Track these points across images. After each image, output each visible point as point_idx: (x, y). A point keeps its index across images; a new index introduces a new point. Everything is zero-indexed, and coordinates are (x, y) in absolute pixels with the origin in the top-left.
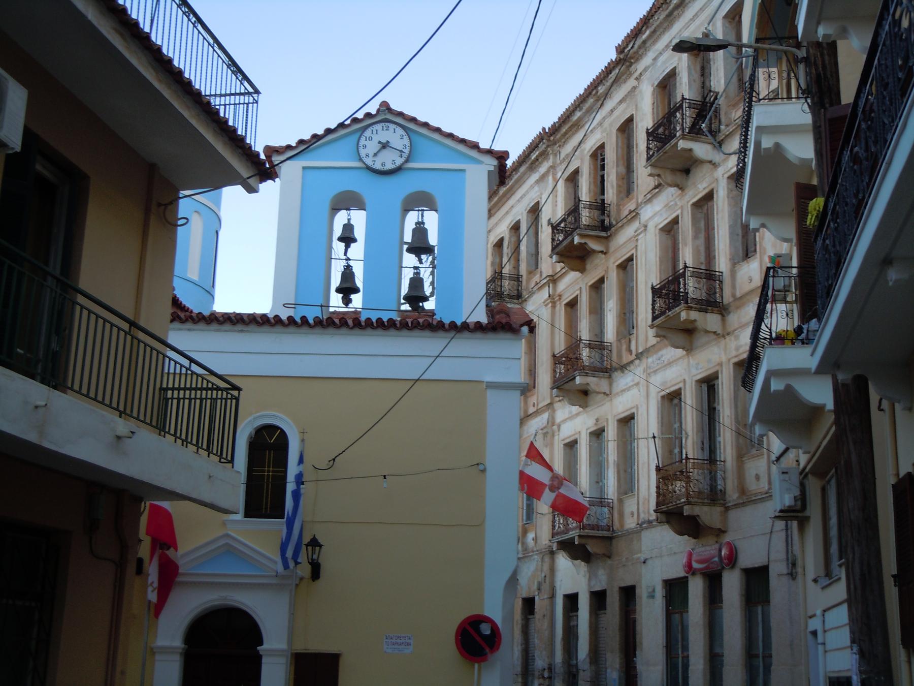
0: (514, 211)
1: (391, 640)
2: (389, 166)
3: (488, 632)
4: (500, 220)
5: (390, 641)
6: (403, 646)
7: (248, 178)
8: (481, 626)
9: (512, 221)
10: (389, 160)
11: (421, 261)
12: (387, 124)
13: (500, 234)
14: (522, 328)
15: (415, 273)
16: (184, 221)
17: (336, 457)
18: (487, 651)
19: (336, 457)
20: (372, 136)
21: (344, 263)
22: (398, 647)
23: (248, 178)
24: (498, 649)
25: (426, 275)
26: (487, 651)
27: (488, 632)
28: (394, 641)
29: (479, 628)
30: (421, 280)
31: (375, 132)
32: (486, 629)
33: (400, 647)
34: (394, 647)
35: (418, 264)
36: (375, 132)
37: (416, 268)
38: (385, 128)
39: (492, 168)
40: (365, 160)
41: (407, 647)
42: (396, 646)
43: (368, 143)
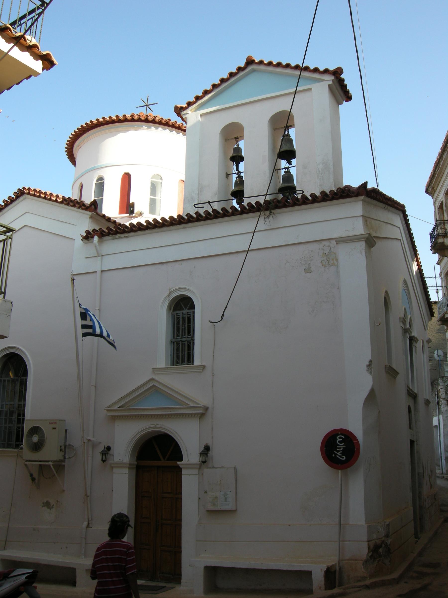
9: (445, 190)
11: (290, 163)
15: (285, 172)
17: (224, 312)
19: (224, 312)
25: (293, 171)
30: (292, 176)
35: (288, 165)
37: (288, 168)
39: (331, 82)
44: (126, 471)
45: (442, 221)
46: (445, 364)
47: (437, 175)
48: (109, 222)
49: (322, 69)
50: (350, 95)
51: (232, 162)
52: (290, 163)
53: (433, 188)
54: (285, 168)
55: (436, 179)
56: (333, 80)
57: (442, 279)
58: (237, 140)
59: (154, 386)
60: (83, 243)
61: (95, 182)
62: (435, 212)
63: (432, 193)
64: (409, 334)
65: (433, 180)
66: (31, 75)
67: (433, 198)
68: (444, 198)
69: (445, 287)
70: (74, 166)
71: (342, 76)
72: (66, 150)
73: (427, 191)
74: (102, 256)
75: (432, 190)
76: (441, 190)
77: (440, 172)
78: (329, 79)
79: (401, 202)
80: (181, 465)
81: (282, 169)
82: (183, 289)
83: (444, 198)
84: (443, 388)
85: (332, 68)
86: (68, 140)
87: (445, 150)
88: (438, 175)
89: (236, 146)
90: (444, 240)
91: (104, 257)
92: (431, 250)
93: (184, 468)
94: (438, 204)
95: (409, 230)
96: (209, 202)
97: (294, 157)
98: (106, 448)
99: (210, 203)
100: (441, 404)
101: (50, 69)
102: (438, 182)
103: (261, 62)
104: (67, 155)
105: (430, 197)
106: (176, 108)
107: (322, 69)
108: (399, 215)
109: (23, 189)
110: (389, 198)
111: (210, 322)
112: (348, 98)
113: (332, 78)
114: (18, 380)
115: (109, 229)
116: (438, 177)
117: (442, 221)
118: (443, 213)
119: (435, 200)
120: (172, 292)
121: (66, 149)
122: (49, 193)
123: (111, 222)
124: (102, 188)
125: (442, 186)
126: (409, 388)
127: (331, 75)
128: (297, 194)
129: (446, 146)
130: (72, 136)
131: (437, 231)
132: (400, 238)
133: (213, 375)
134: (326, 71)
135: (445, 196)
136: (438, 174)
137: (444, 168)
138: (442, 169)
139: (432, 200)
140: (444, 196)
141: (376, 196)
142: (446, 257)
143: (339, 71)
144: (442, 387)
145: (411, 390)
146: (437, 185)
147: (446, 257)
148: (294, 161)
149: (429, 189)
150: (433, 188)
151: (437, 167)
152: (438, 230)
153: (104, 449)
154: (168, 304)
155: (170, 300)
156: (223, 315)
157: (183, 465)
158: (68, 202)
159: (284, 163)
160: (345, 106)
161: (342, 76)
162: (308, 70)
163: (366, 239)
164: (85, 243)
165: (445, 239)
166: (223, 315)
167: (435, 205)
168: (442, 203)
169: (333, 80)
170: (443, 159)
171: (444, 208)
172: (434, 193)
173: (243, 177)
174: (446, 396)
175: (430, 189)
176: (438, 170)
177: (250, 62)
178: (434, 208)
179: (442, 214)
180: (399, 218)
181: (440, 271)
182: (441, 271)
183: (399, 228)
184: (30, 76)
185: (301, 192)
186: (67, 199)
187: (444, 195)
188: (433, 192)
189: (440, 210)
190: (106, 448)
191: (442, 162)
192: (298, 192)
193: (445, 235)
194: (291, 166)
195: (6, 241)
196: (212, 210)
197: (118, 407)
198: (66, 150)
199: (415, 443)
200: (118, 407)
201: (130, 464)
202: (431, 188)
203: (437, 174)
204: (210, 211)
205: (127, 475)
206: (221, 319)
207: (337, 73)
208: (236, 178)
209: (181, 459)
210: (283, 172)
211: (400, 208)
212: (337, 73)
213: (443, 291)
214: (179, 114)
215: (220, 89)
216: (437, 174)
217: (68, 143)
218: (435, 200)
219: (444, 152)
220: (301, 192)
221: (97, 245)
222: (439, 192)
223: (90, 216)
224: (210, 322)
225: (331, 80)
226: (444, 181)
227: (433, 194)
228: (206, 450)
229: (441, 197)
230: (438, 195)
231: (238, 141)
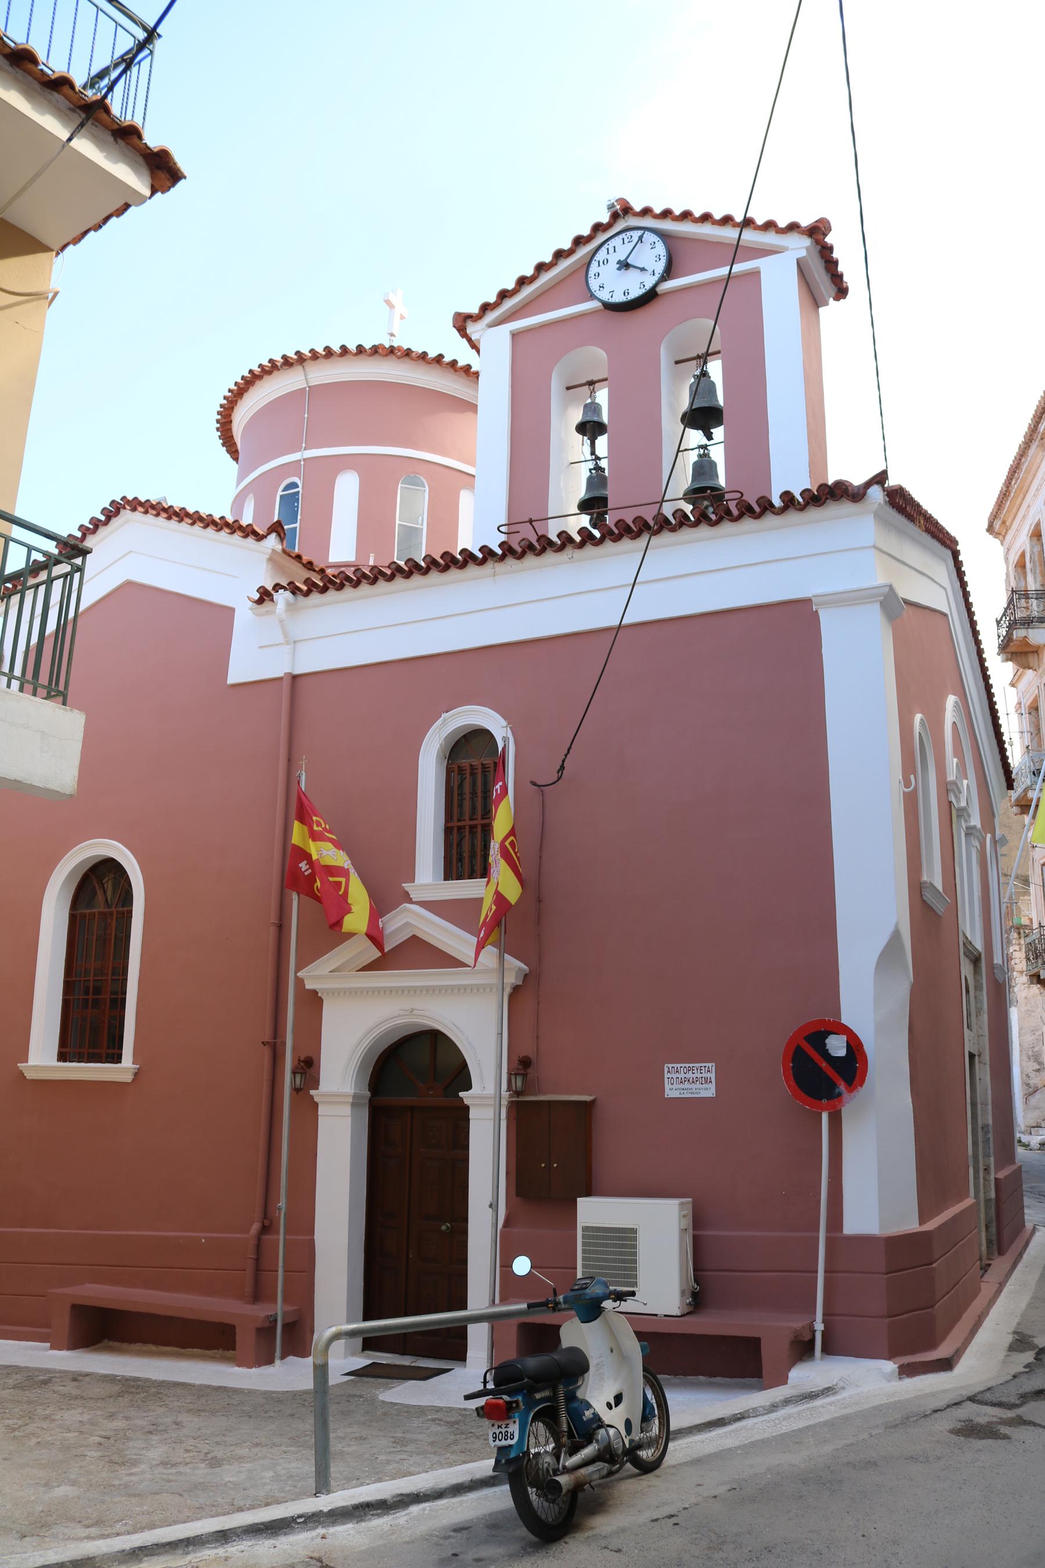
0: (1032, 511)
1: (677, 1075)
2: (636, 293)
3: (842, 1052)
4: (1017, 530)
5: (675, 1076)
6: (698, 1085)
7: (70, 139)
8: (827, 1041)
9: (1031, 525)
10: (633, 286)
11: (709, 437)
12: (629, 234)
13: (1020, 547)
14: (869, 491)
15: (700, 456)
16: (503, 529)
17: (564, 761)
18: (842, 1087)
19: (564, 761)
20: (608, 257)
21: (591, 465)
22: (690, 1086)
23: (70, 139)
24: (862, 1083)
25: (717, 454)
26: (842, 1087)
27: (842, 1052)
28: (682, 1075)
29: (825, 1045)
30: (713, 465)
31: (611, 250)
32: (837, 1046)
33: (693, 1086)
34: (682, 1086)
35: (704, 441)
36: (611, 250)
37: (704, 447)
38: (626, 241)
39: (803, 253)
40: (598, 294)
41: (705, 1086)
42: (686, 1085)
43: (602, 269)
44: (347, 1110)
45: (1022, 593)
46: (1022, 900)
47: (1012, 494)
48: (311, 570)
49: (782, 224)
50: (844, 284)
51: (581, 436)
52: (709, 437)
53: (1004, 522)
54: (701, 447)
55: (1011, 502)
56: (807, 249)
57: (1022, 714)
58: (592, 387)
59: (407, 923)
60: (254, 616)
61: (280, 493)
62: (1008, 575)
63: (1000, 534)
64: (966, 821)
65: (1005, 505)
66: (129, 203)
67: (1002, 544)
68: (1028, 541)
69: (1028, 732)
70: (235, 462)
71: (829, 239)
72: (218, 425)
73: (990, 529)
74: (295, 642)
75: (1000, 526)
76: (1020, 525)
77: (1020, 488)
78: (800, 246)
79: (953, 532)
80: (466, 1097)
81: (692, 449)
82: (425, 1018)
83: (1027, 543)
84: (1020, 950)
85: (805, 222)
86: (183, 180)
87: (1032, 439)
88: (1015, 493)
89: (589, 401)
90: (1028, 632)
91: (298, 644)
92: (999, 654)
93: (474, 1105)
94: (1014, 557)
95: (966, 595)
96: (531, 521)
97: (719, 422)
98: (302, 1062)
99: (533, 523)
100: (1014, 985)
101: (169, 189)
102: (1015, 510)
103: (646, 212)
104: (219, 437)
105: (997, 542)
106: (457, 315)
107: (782, 224)
108: (944, 560)
109: (121, 500)
110: (928, 516)
111: (534, 784)
112: (842, 292)
113: (807, 242)
114: (112, 914)
115: (310, 582)
116: (1015, 497)
117: (1022, 593)
118: (1025, 578)
119: (1008, 550)
120: (448, 718)
121: (218, 414)
122: (178, 507)
123: (314, 571)
124: (296, 504)
125: (1024, 517)
126: (967, 938)
127: (804, 236)
128: (727, 501)
129: (1036, 429)
130: (230, 394)
131: (1012, 613)
132: (946, 610)
133: (540, 901)
134: (793, 227)
135: (1031, 540)
136: (1016, 490)
137: (1030, 478)
138: (1024, 480)
139: (1002, 548)
140: (1029, 539)
141: (904, 506)
142: (1031, 670)
143: (821, 226)
144: (1017, 948)
145: (971, 943)
146: (1012, 516)
147: (1029, 668)
148: (718, 433)
149: (994, 525)
150: (1004, 522)
151: (1014, 475)
152: (1015, 611)
153: (299, 1064)
154: (438, 746)
155: (444, 737)
156: (562, 767)
157: (473, 1097)
158: (219, 527)
159: (695, 437)
160: (832, 312)
161: (829, 239)
162: (752, 225)
163: (882, 598)
164: (258, 615)
165: (1030, 630)
166: (562, 767)
167: (1006, 559)
168: (1023, 555)
169: (807, 249)
170: (1029, 458)
171: (1028, 566)
172: (1006, 533)
173: (604, 469)
174: (1027, 965)
175: (997, 525)
176: (1015, 484)
177: (622, 211)
178: (1005, 565)
179: (1022, 579)
180: (945, 569)
181: (1016, 701)
182: (1019, 699)
183: (945, 589)
184: (127, 206)
185: (738, 495)
186: (219, 521)
187: (1027, 535)
188: (1004, 531)
189: (1019, 570)
190: (302, 1062)
191: (1026, 465)
192: (727, 497)
193: (1028, 622)
194: (712, 442)
195: (69, 577)
196: (536, 537)
197: (330, 972)
198: (218, 425)
199: (977, 1057)
200: (330, 972)
201: (355, 1096)
202: (999, 523)
203: (1014, 490)
204: (533, 539)
205: (350, 1118)
206: (556, 779)
207: (818, 231)
208: (590, 470)
209: (468, 1086)
210: (693, 457)
211: (948, 542)
212: (818, 231)
213: (1023, 742)
214: (462, 331)
215: (557, 271)
216: (1014, 490)
217: (222, 409)
218: (1008, 550)
219: (1031, 442)
220: (739, 495)
221: (284, 616)
222: (1017, 530)
223: (268, 557)
224: (534, 784)
225: (803, 248)
226: (1029, 506)
227: (1004, 537)
228: (521, 1067)
229: (1022, 541)
230: (1015, 537)
231: (593, 389)
